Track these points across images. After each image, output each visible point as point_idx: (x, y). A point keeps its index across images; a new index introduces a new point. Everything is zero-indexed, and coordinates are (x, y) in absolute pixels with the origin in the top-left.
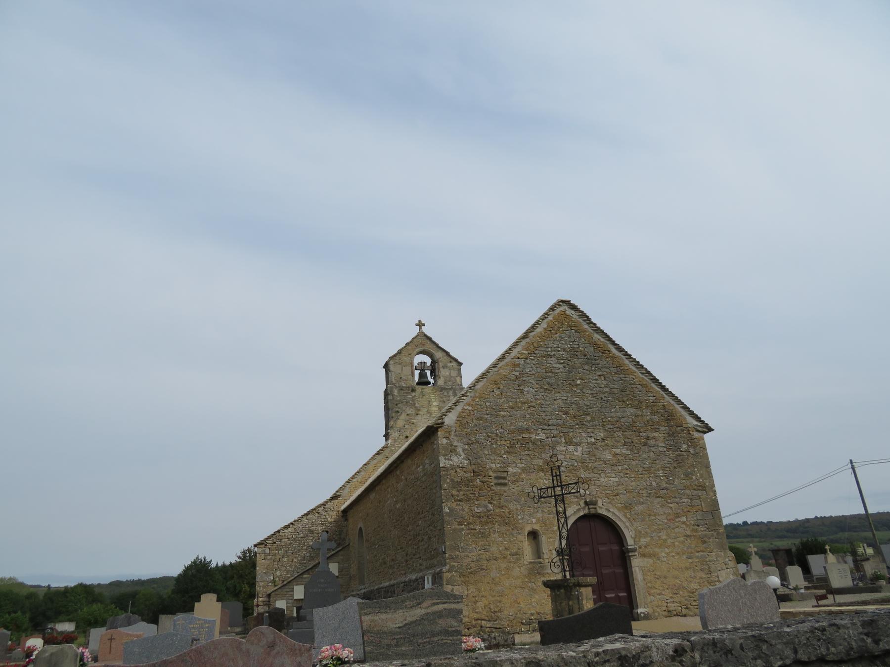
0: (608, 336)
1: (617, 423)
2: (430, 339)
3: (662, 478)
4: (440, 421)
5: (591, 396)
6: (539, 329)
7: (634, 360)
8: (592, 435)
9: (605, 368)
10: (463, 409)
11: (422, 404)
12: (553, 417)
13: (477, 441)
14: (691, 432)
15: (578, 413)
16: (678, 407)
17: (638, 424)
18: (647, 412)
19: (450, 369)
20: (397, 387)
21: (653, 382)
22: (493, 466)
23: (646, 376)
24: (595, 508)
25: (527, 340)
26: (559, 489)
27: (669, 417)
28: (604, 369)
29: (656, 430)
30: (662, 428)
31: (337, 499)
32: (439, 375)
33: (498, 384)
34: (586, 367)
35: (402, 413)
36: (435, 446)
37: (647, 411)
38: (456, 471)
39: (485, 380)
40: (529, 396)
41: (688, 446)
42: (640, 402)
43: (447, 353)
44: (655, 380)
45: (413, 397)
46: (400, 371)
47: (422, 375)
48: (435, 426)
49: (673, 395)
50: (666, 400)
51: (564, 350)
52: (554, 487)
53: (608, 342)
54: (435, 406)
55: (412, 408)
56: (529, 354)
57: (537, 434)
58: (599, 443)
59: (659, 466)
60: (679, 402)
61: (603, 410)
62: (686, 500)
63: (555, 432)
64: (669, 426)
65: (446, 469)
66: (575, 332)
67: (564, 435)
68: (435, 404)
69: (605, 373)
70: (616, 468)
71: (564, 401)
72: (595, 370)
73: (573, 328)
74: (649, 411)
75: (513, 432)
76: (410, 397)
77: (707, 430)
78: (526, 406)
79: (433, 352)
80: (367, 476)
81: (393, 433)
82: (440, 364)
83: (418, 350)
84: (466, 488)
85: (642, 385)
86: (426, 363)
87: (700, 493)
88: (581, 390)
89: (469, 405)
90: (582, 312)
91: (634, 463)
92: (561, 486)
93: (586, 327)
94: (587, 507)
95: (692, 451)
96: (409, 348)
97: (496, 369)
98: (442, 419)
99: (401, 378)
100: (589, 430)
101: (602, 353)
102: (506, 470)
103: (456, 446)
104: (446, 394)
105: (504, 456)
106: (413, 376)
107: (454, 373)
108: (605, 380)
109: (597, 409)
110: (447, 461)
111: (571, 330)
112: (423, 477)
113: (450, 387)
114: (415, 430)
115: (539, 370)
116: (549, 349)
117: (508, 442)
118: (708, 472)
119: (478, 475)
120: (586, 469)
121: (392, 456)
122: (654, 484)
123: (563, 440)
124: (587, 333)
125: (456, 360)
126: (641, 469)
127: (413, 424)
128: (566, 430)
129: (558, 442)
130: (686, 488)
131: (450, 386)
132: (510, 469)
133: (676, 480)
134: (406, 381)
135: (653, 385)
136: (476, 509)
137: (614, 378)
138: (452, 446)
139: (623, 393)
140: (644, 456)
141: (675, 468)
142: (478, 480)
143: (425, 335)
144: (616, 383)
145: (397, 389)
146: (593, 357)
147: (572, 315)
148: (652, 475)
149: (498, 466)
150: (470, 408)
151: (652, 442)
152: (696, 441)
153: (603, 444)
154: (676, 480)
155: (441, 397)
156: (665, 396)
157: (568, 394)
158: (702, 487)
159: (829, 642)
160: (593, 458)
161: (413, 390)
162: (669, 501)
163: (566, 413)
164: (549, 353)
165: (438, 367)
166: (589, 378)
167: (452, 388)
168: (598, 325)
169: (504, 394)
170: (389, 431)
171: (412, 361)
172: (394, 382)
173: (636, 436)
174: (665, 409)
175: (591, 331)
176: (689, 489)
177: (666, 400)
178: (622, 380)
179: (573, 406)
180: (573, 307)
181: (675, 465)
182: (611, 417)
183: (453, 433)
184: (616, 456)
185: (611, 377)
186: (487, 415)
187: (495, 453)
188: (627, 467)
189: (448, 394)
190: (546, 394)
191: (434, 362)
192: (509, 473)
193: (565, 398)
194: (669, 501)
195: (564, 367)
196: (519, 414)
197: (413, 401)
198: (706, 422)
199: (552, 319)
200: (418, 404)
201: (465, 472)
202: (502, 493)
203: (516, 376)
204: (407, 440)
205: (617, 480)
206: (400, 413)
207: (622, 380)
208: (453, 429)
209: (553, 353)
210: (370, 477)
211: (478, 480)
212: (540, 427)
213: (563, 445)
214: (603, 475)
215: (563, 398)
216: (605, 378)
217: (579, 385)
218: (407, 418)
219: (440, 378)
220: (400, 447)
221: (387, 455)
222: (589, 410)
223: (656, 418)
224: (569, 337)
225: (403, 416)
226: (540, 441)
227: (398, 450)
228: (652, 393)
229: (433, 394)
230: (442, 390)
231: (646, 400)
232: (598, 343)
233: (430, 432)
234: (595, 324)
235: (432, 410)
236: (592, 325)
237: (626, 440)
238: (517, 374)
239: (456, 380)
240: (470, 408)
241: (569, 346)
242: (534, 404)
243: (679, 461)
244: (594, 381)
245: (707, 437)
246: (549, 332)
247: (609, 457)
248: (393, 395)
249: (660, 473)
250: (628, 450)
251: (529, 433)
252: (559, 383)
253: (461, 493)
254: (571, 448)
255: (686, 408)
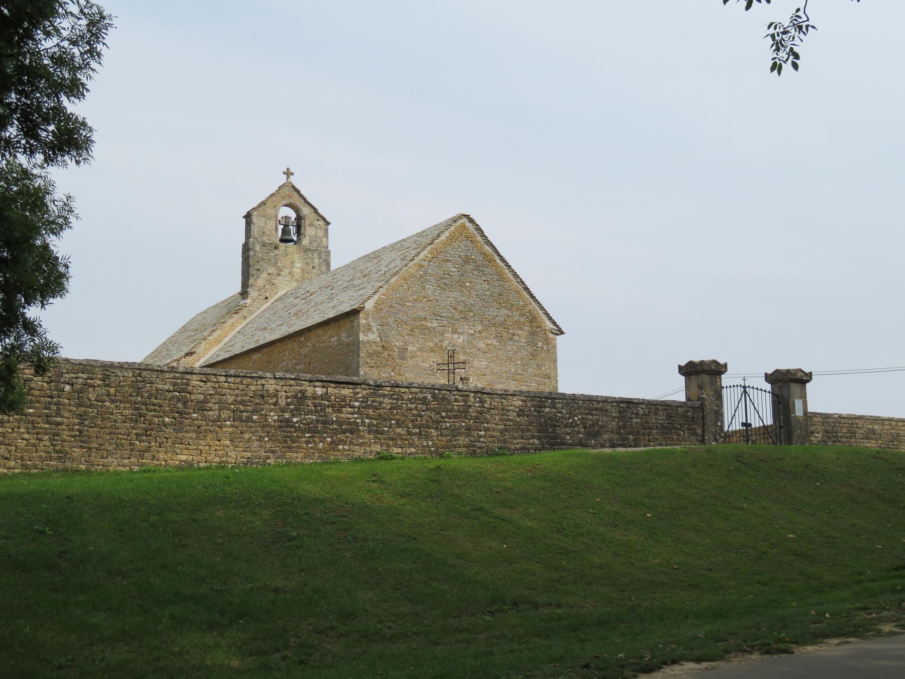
0: (495, 249)
1: (493, 320)
2: (298, 191)
3: (519, 366)
4: (362, 306)
5: (475, 297)
6: (443, 237)
7: (513, 271)
8: (472, 327)
9: (489, 274)
10: (380, 298)
11: (285, 264)
12: (445, 311)
13: (387, 324)
14: (547, 334)
15: (464, 310)
16: (541, 312)
17: (508, 323)
18: (517, 313)
19: (316, 228)
20: (259, 242)
21: (525, 290)
22: (398, 344)
23: (520, 285)
24: (467, 383)
25: (432, 246)
26: (452, 365)
27: (533, 319)
28: (488, 276)
29: (521, 329)
30: (526, 328)
31: (191, 356)
32: (304, 234)
33: (407, 280)
34: (475, 273)
35: (263, 271)
36: (355, 324)
37: (517, 313)
38: (371, 345)
39: (397, 276)
40: (429, 292)
41: (543, 343)
42: (512, 305)
43: (315, 210)
44: (526, 289)
45: (276, 255)
46: (264, 225)
47: (285, 231)
48: (358, 309)
49: (539, 303)
50: (532, 306)
51: (460, 256)
52: (448, 364)
53: (494, 253)
54: (299, 268)
55: (274, 268)
56: (432, 257)
57: (432, 323)
58: (477, 334)
59: (519, 357)
60: (542, 308)
61: (483, 309)
62: (534, 385)
63: (445, 322)
64: (531, 327)
65: (364, 343)
66: (470, 242)
67: (451, 326)
68: (298, 265)
69: (489, 279)
70: (486, 355)
71: (455, 299)
72: (481, 276)
73: (469, 239)
74: (518, 313)
75: (414, 320)
76: (273, 254)
77: (559, 333)
78: (426, 300)
79: (300, 206)
80: (224, 335)
81: (253, 293)
82: (307, 221)
83: (284, 202)
84: (377, 358)
85: (515, 292)
86: (291, 218)
87: (546, 380)
88: (469, 291)
89: (384, 295)
90: (478, 226)
91: (500, 353)
92: (454, 363)
93: (479, 238)
94: (461, 382)
95: (545, 348)
96: (275, 199)
97: (406, 268)
98: (364, 304)
99: (264, 232)
100: (471, 324)
101: (489, 262)
102: (406, 347)
103: (372, 326)
104: (310, 255)
105: (406, 337)
106: (276, 232)
107: (320, 233)
108: (488, 284)
109: (478, 307)
110: (365, 337)
111: (468, 240)
112: (337, 346)
113: (315, 248)
114: (275, 291)
115: (439, 271)
116: (449, 255)
117: (410, 327)
118: (554, 365)
119: (386, 350)
120: (465, 353)
121: (250, 316)
122: (513, 370)
123: (450, 329)
124: (480, 244)
125: (324, 219)
126: (505, 358)
127: (274, 284)
128: (453, 322)
129: (446, 331)
130: (536, 375)
131: (315, 247)
132: (410, 348)
133: (530, 369)
134: (269, 236)
135: (525, 293)
136: (382, 374)
137: (495, 284)
138: (369, 325)
139: (500, 297)
140: (509, 348)
141: (530, 359)
142: (386, 353)
143: (293, 187)
144: (496, 288)
145: (260, 244)
146: (481, 265)
147: (469, 228)
148: (512, 363)
149: (401, 344)
150: (385, 297)
151: (516, 338)
152: (549, 340)
153: (479, 336)
154: (530, 369)
155: (305, 259)
156: (532, 302)
157: (459, 294)
158: (548, 377)
159: (542, 394)
160: (471, 346)
161: (276, 248)
162: (522, 384)
163: (455, 309)
164: (448, 258)
165: (304, 224)
166: (476, 282)
167: (317, 249)
168: (489, 239)
169: (410, 289)
170: (249, 290)
171: (277, 214)
172: (256, 236)
173: (505, 332)
174: (530, 313)
175: (483, 242)
176: (538, 377)
177: (532, 306)
178: (501, 286)
179: (461, 303)
180: (471, 221)
181: (531, 357)
182: (489, 315)
183: (370, 316)
184: (488, 346)
185: (493, 283)
186: (397, 304)
187: (400, 334)
188: (495, 355)
189: (312, 256)
190: (442, 292)
191: (299, 218)
192: (408, 350)
193: (456, 296)
194: (522, 384)
195: (458, 271)
196: (420, 305)
197: (276, 259)
198: (557, 324)
199: (453, 229)
200: (281, 263)
201: (377, 346)
202: (402, 364)
203: (421, 275)
204: (266, 301)
205: (486, 364)
206: (261, 271)
207: (501, 286)
208: (371, 312)
209: (451, 259)
210: (226, 336)
211: (386, 353)
212: (435, 317)
213: (450, 333)
214: (476, 360)
215: (454, 296)
216: (488, 283)
217: (467, 287)
218: (268, 277)
219: (305, 237)
220: (259, 308)
221: (245, 315)
222: (473, 308)
223: (522, 319)
224: (465, 246)
225: (264, 275)
226: (434, 329)
227: (256, 311)
228: (523, 299)
229: (297, 254)
230: (307, 250)
231: (517, 304)
232: (487, 253)
233: (355, 312)
234: (486, 237)
235: (295, 272)
236: (484, 238)
237: (498, 335)
238: (422, 273)
239: (322, 241)
240: (385, 297)
241: (464, 254)
242: (432, 299)
243: (534, 355)
244: (480, 285)
245: (559, 338)
246: (449, 240)
247: (483, 346)
248: (255, 251)
249: (519, 362)
250: (497, 342)
251: (426, 321)
252: (453, 284)
253: (373, 361)
254: (455, 336)
255: (547, 314)
